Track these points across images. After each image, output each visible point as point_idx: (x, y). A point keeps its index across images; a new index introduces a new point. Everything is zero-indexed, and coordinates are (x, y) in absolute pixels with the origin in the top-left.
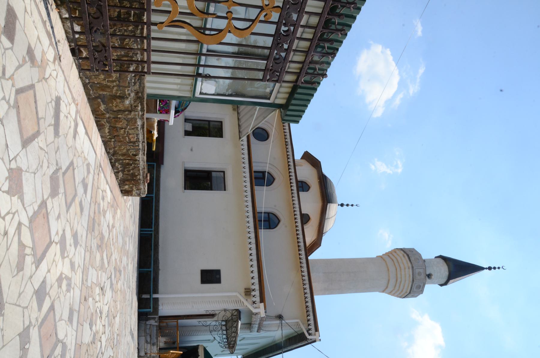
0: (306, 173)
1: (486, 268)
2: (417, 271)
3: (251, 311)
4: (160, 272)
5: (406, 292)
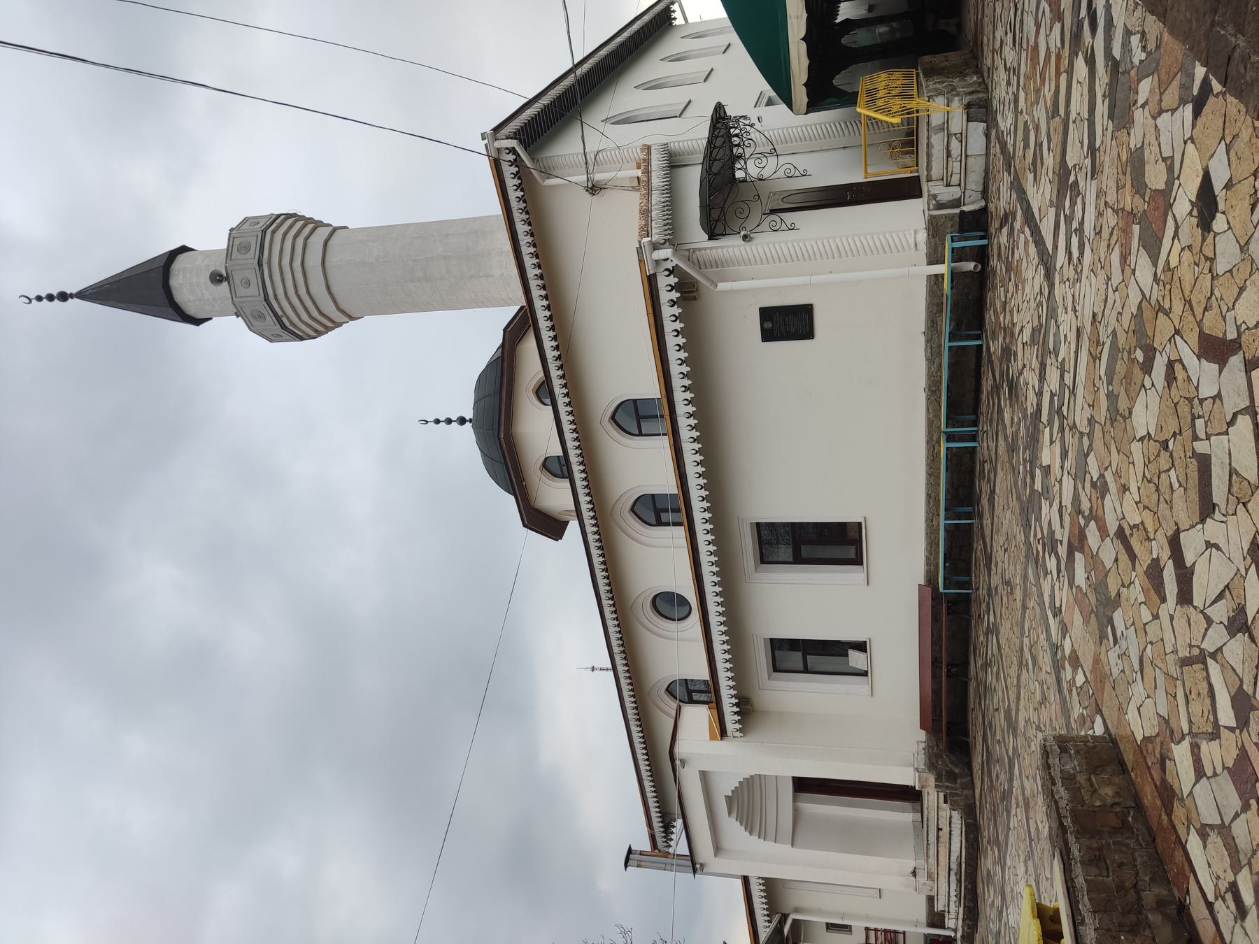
0: (556, 496)
1: (72, 296)
2: (254, 289)
5: (273, 232)
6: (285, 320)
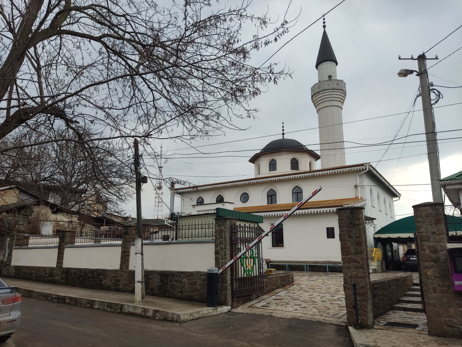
1: (324, 29)
2: (327, 87)
3: (367, 172)
4: (330, 260)
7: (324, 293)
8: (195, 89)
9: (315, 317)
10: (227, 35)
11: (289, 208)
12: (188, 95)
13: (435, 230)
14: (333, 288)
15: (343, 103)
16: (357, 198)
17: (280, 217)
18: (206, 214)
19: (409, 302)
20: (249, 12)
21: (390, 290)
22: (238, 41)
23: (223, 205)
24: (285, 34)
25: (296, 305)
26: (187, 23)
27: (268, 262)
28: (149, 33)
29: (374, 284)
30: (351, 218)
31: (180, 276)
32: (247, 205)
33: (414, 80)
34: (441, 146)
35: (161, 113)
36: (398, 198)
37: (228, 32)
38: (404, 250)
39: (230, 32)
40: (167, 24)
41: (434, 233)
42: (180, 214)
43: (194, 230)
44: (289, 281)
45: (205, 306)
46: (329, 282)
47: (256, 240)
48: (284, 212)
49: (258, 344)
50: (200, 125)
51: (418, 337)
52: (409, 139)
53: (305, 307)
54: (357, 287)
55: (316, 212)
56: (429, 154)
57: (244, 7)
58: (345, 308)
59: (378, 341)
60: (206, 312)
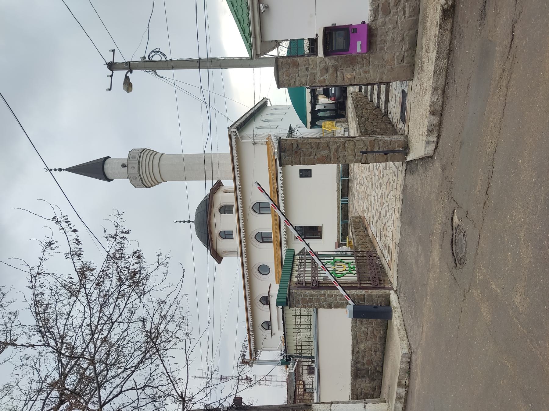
1: (64, 170)
2: (136, 170)
3: (238, 130)
6: (143, 180)
7: (372, 184)
8: (125, 334)
9: (398, 195)
10: (58, 291)
11: (278, 218)
12: (132, 344)
13: (304, 68)
14: (365, 174)
15: (157, 153)
16: (267, 144)
17: (287, 228)
18: (283, 319)
19: (379, 98)
20: (35, 263)
21: (367, 116)
22: (70, 278)
23: (272, 297)
24: (69, 219)
25: (386, 216)
26: (40, 343)
27: (339, 245)
28: (43, 396)
29: (361, 132)
30: (289, 152)
31: (358, 352)
32: (272, 267)
33: (136, 76)
34: (213, 55)
35: (152, 379)
36: (268, 101)
37: (55, 290)
38: (324, 98)
39: (55, 287)
40: (35, 370)
41: (307, 69)
42: (282, 352)
43: (303, 335)
44: (359, 222)
45: (391, 322)
46: (360, 178)
47: (315, 258)
48: (282, 224)
49: (431, 260)
50: (171, 327)
51: (416, 91)
52: (205, 87)
53: (388, 205)
54: (364, 150)
55: (282, 189)
56: (221, 67)
57: (28, 269)
58: (388, 163)
59: (421, 132)
60: (398, 320)
